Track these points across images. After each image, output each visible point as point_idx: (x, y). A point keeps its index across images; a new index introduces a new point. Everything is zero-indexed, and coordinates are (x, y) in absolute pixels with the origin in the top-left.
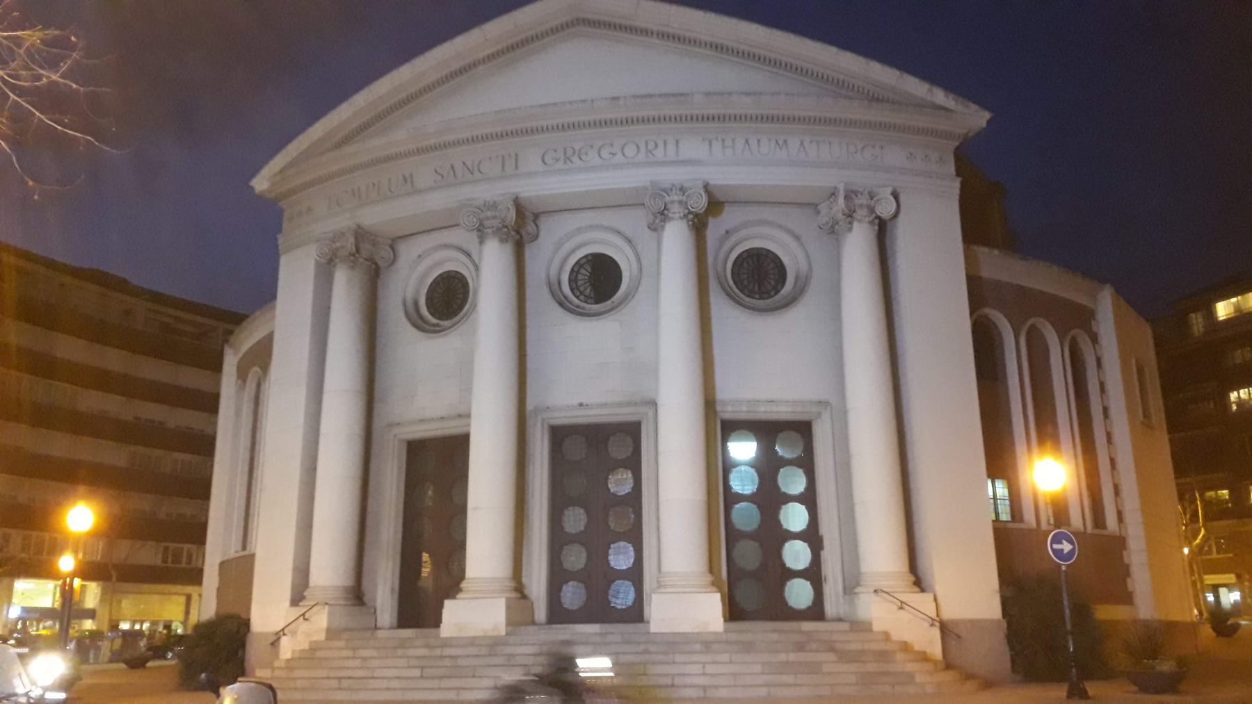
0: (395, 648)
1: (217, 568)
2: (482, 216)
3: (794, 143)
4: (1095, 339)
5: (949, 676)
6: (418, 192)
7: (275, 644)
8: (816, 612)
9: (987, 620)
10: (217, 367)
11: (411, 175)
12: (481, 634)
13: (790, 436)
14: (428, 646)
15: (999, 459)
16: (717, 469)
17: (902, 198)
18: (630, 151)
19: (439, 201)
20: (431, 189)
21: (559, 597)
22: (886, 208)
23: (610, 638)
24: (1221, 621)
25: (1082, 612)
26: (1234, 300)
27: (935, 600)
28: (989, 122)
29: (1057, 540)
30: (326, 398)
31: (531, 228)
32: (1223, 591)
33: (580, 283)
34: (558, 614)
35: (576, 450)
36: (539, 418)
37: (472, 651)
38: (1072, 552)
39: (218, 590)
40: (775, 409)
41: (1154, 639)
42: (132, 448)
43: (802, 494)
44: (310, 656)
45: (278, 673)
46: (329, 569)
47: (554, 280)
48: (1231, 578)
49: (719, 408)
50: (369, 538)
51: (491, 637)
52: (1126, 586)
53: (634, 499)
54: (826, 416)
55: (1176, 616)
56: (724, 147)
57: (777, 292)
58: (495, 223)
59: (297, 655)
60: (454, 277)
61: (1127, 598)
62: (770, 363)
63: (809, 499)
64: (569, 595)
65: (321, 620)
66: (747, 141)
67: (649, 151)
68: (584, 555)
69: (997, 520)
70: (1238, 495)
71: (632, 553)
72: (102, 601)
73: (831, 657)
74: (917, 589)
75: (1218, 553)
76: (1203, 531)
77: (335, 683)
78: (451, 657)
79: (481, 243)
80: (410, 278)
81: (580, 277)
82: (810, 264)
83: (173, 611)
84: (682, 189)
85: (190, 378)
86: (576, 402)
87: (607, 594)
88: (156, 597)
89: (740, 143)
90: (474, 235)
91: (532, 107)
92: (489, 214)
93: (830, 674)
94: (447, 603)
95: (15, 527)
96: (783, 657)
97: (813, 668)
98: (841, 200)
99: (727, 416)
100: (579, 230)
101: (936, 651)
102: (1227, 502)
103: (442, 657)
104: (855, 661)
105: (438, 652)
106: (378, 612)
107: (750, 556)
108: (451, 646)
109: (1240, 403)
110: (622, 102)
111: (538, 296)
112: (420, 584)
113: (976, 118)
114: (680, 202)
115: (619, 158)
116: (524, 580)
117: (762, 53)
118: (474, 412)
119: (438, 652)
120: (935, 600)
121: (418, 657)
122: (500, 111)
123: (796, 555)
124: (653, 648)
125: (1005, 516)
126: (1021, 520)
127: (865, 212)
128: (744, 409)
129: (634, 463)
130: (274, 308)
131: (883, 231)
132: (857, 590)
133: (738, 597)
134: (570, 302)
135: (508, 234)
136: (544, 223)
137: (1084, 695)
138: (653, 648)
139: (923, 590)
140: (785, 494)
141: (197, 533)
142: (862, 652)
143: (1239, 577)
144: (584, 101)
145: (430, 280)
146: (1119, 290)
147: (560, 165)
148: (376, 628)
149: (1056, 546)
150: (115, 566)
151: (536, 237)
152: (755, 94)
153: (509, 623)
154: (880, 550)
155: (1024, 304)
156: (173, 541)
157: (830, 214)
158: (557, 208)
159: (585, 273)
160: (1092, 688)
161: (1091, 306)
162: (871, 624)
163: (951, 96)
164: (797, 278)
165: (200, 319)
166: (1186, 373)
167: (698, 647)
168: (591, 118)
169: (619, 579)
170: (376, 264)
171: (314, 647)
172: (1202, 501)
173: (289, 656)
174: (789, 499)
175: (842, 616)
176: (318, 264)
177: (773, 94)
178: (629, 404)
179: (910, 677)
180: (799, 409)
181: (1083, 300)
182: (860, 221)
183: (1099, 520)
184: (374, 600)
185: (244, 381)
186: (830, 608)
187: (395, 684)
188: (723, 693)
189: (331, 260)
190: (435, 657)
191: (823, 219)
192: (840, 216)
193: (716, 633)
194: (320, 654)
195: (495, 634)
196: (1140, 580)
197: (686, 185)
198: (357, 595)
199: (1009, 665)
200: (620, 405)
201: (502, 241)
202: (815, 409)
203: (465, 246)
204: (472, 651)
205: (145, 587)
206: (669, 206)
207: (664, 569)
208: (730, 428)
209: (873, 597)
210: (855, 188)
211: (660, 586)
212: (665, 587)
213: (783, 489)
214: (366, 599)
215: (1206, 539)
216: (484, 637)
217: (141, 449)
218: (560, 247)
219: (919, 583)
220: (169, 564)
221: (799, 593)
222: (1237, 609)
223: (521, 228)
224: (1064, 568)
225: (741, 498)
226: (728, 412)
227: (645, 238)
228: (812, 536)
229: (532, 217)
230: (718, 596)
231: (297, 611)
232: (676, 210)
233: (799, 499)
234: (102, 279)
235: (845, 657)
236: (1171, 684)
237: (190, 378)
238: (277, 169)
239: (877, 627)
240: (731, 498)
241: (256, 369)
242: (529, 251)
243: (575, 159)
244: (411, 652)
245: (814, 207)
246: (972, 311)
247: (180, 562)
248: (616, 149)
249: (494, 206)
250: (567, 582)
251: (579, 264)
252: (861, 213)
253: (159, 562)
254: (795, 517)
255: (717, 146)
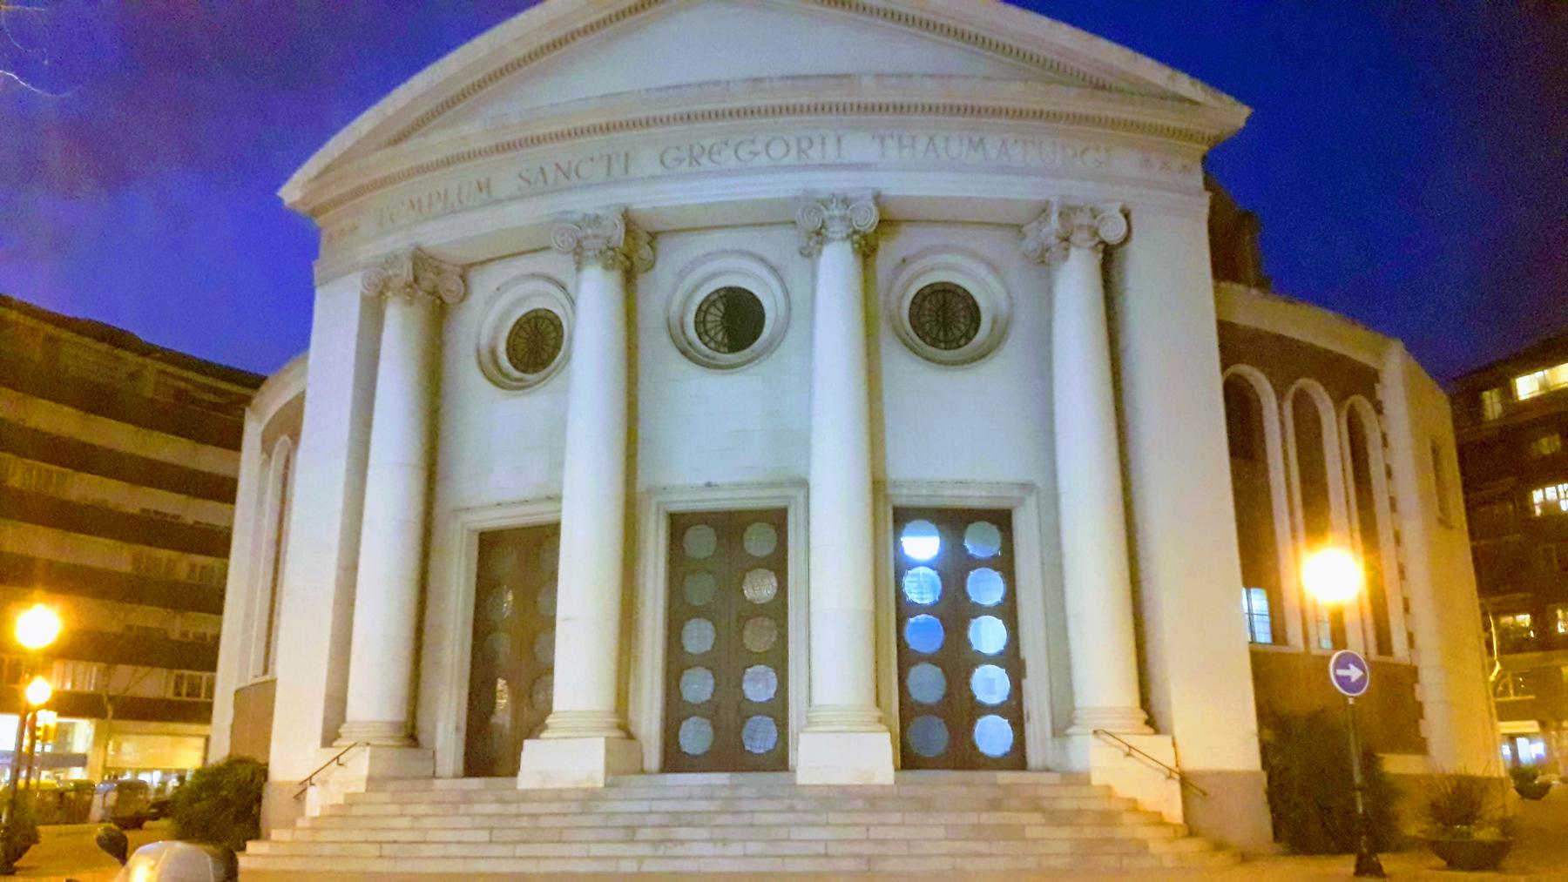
0: (455, 804)
1: (231, 699)
2: (581, 234)
3: (993, 144)
4: (1379, 408)
5: (1193, 846)
6: (499, 202)
7: (300, 797)
8: (1017, 759)
9: (1240, 773)
10: (233, 441)
11: (488, 180)
12: (571, 785)
13: (982, 527)
14: (502, 801)
15: (1257, 561)
16: (891, 570)
17: (1133, 216)
18: (777, 150)
19: (520, 216)
20: (512, 199)
21: (677, 736)
22: (1113, 231)
23: (743, 792)
24: (1526, 781)
25: (1370, 760)
26: (1539, 374)
27: (1174, 744)
28: (1248, 121)
29: (1342, 663)
30: (371, 473)
31: (645, 252)
32: (1522, 743)
33: (709, 326)
34: (674, 760)
35: (701, 543)
36: (654, 502)
37: (556, 807)
38: (1359, 684)
39: (233, 727)
40: (963, 492)
41: (1459, 802)
42: (138, 548)
43: (999, 605)
44: (342, 814)
45: (299, 835)
46: (374, 696)
47: (675, 322)
48: (1532, 726)
49: (890, 491)
50: (426, 662)
51: (585, 790)
52: (1417, 730)
53: (777, 611)
54: (1031, 503)
55: (1477, 769)
56: (901, 146)
57: (969, 339)
58: (599, 244)
59: (327, 812)
60: (544, 318)
61: (1419, 746)
62: (959, 430)
63: (1008, 611)
64: (690, 735)
65: (359, 766)
66: (931, 139)
67: (801, 151)
68: (711, 682)
69: (1253, 642)
70: (1543, 621)
71: (774, 681)
72: (95, 744)
73: (1037, 818)
74: (1148, 730)
75: (1516, 694)
76: (1498, 667)
77: (373, 850)
78: (531, 816)
79: (579, 268)
80: (487, 316)
81: (709, 318)
82: (1012, 305)
83: (169, 758)
84: (846, 201)
85: (208, 459)
86: (702, 482)
87: (739, 733)
88: (168, 739)
89: (922, 143)
90: (570, 258)
91: (648, 90)
92: (590, 232)
93: (1035, 840)
94: (527, 744)
95: (170, 701)
96: (972, 818)
97: (1014, 833)
98: (1054, 218)
99: (902, 502)
100: (708, 257)
101: (1175, 813)
102: (1527, 630)
103: (518, 815)
104: (1070, 824)
105: (512, 809)
106: (438, 756)
107: (928, 683)
108: (534, 801)
109: (1545, 505)
110: (767, 84)
111: (656, 343)
112: (494, 720)
113: (1232, 115)
114: (843, 218)
115: (762, 160)
116: (631, 715)
117: (953, 24)
118: (567, 493)
119: (512, 809)
120: (1174, 744)
121: (488, 816)
122: (604, 96)
123: (990, 684)
124: (799, 805)
125: (1264, 636)
126: (1285, 642)
127: (1085, 235)
128: (924, 492)
129: (778, 564)
130: (306, 358)
131: (1109, 259)
132: (1070, 731)
133: (912, 739)
134: (698, 351)
135: (613, 259)
136: (663, 245)
137: (1377, 871)
138: (799, 805)
139: (1157, 732)
140: (975, 604)
141: (205, 655)
142: (1079, 812)
143: (1543, 724)
144: (716, 83)
145: (514, 320)
146: (1412, 347)
147: (685, 167)
148: (434, 776)
149: (1341, 672)
150: (112, 699)
151: (652, 265)
152: (942, 77)
153: (609, 770)
154: (1103, 679)
155: (1287, 359)
156: (188, 667)
157: (1036, 240)
158: (679, 226)
159: (715, 315)
160: (1388, 862)
161: (1376, 366)
162: (1088, 775)
163: (1199, 85)
164: (994, 322)
165: (224, 386)
166: (1492, 463)
167: (860, 803)
168: (726, 106)
169: (757, 714)
170: (440, 298)
171: (351, 801)
172: (1497, 628)
173: (317, 813)
174: (932, 659)
175: (1050, 765)
176: (364, 299)
177: (966, 77)
178: (772, 485)
179: (1142, 848)
180: (995, 493)
181: (1361, 357)
182: (1078, 247)
183: (1384, 645)
184: (433, 738)
185: (270, 456)
186: (1034, 755)
187: (453, 850)
188: (892, 865)
189: (381, 293)
190: (510, 816)
191: (1030, 244)
192: (1053, 240)
193: (883, 786)
194: (357, 811)
195: (590, 785)
196: (1434, 725)
197: (851, 195)
198: (411, 734)
199: (1269, 830)
200: (760, 485)
201: (606, 267)
202: (1016, 493)
203: (558, 277)
204: (556, 807)
205: (153, 726)
206: (828, 223)
207: (816, 700)
208: (903, 517)
209: (1092, 738)
210: (1073, 203)
211: (810, 723)
212: (817, 724)
213: (973, 599)
214: (422, 738)
215: (1501, 676)
216: (577, 789)
217: (146, 549)
218: (685, 280)
219: (1153, 722)
220: (184, 698)
221: (992, 735)
222: (1541, 764)
223: (633, 251)
224: (1351, 701)
225: (917, 609)
226: (905, 497)
227: (797, 271)
228: (1012, 660)
229: (646, 237)
230: (888, 735)
231: (331, 753)
232: (837, 229)
233: (995, 611)
234: (115, 338)
235: (1056, 818)
236: (1489, 858)
237: (208, 459)
238: (315, 172)
239: (1097, 780)
240: (904, 609)
241: (285, 438)
242: (643, 282)
243: (704, 160)
244: (477, 808)
245: (1018, 229)
246: (1225, 366)
247: (199, 696)
248: (759, 147)
249: (596, 220)
250: (687, 718)
251: (708, 302)
252: (1080, 236)
253: (170, 695)
254: (988, 635)
255: (891, 144)
